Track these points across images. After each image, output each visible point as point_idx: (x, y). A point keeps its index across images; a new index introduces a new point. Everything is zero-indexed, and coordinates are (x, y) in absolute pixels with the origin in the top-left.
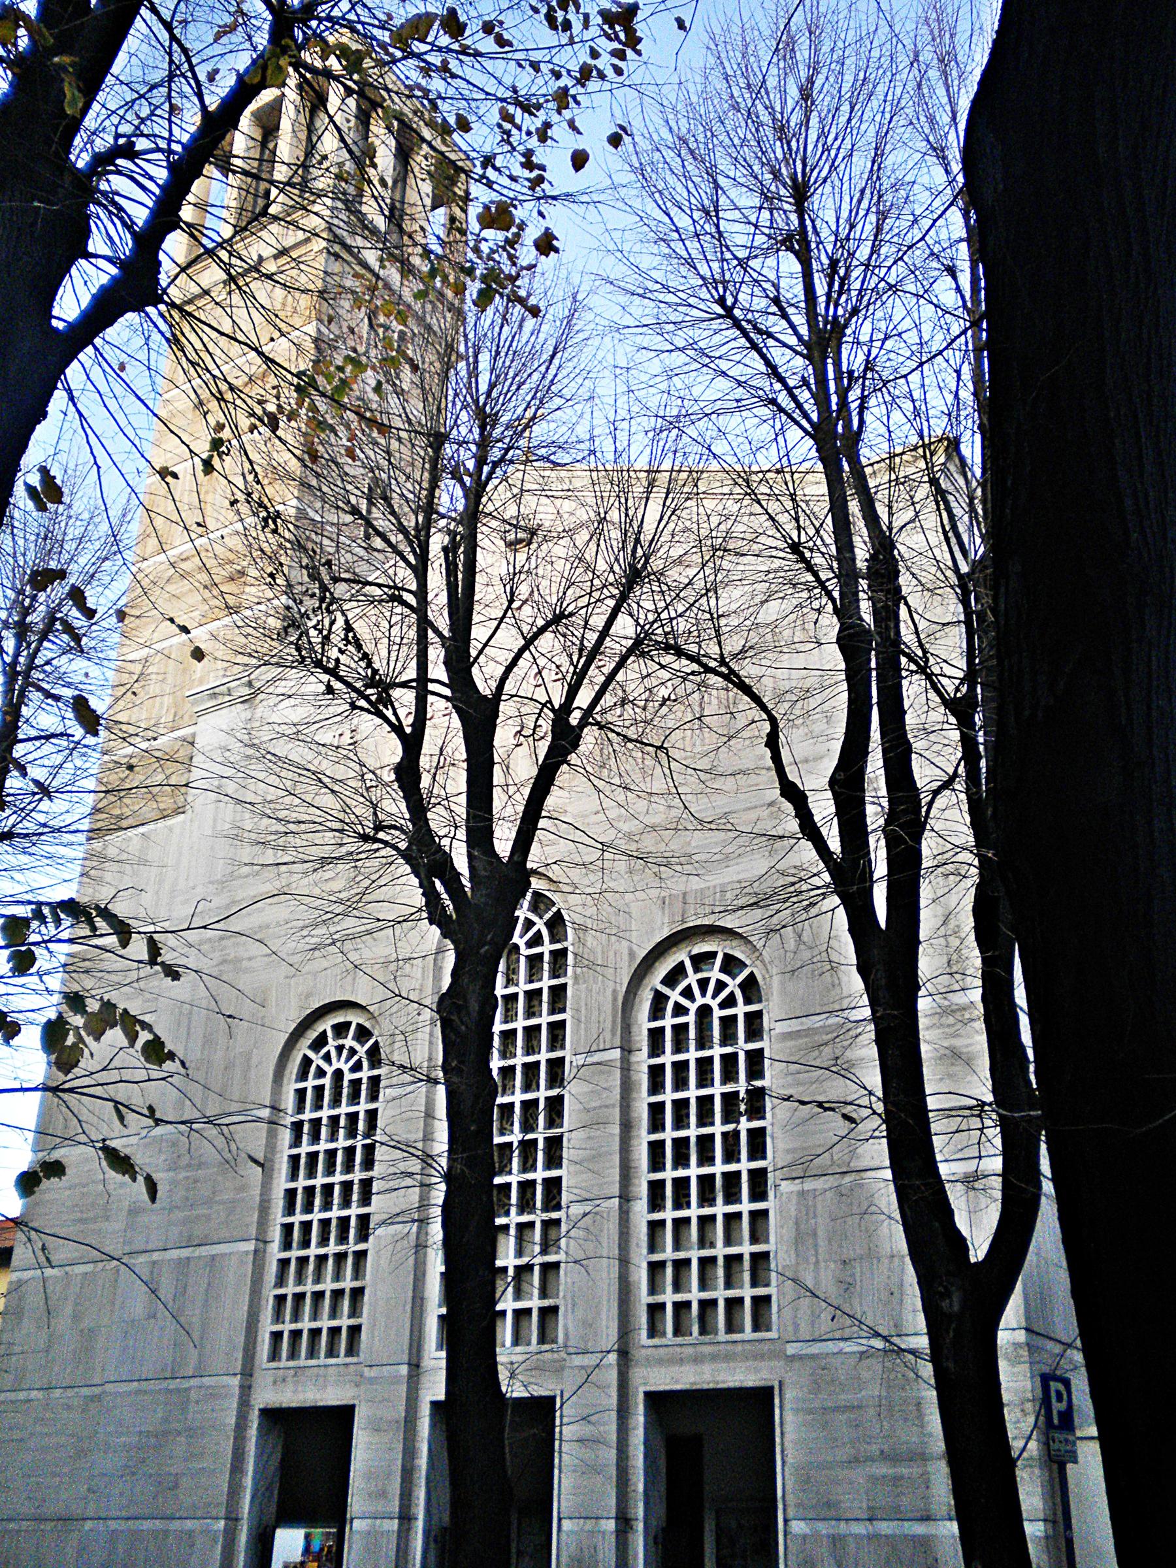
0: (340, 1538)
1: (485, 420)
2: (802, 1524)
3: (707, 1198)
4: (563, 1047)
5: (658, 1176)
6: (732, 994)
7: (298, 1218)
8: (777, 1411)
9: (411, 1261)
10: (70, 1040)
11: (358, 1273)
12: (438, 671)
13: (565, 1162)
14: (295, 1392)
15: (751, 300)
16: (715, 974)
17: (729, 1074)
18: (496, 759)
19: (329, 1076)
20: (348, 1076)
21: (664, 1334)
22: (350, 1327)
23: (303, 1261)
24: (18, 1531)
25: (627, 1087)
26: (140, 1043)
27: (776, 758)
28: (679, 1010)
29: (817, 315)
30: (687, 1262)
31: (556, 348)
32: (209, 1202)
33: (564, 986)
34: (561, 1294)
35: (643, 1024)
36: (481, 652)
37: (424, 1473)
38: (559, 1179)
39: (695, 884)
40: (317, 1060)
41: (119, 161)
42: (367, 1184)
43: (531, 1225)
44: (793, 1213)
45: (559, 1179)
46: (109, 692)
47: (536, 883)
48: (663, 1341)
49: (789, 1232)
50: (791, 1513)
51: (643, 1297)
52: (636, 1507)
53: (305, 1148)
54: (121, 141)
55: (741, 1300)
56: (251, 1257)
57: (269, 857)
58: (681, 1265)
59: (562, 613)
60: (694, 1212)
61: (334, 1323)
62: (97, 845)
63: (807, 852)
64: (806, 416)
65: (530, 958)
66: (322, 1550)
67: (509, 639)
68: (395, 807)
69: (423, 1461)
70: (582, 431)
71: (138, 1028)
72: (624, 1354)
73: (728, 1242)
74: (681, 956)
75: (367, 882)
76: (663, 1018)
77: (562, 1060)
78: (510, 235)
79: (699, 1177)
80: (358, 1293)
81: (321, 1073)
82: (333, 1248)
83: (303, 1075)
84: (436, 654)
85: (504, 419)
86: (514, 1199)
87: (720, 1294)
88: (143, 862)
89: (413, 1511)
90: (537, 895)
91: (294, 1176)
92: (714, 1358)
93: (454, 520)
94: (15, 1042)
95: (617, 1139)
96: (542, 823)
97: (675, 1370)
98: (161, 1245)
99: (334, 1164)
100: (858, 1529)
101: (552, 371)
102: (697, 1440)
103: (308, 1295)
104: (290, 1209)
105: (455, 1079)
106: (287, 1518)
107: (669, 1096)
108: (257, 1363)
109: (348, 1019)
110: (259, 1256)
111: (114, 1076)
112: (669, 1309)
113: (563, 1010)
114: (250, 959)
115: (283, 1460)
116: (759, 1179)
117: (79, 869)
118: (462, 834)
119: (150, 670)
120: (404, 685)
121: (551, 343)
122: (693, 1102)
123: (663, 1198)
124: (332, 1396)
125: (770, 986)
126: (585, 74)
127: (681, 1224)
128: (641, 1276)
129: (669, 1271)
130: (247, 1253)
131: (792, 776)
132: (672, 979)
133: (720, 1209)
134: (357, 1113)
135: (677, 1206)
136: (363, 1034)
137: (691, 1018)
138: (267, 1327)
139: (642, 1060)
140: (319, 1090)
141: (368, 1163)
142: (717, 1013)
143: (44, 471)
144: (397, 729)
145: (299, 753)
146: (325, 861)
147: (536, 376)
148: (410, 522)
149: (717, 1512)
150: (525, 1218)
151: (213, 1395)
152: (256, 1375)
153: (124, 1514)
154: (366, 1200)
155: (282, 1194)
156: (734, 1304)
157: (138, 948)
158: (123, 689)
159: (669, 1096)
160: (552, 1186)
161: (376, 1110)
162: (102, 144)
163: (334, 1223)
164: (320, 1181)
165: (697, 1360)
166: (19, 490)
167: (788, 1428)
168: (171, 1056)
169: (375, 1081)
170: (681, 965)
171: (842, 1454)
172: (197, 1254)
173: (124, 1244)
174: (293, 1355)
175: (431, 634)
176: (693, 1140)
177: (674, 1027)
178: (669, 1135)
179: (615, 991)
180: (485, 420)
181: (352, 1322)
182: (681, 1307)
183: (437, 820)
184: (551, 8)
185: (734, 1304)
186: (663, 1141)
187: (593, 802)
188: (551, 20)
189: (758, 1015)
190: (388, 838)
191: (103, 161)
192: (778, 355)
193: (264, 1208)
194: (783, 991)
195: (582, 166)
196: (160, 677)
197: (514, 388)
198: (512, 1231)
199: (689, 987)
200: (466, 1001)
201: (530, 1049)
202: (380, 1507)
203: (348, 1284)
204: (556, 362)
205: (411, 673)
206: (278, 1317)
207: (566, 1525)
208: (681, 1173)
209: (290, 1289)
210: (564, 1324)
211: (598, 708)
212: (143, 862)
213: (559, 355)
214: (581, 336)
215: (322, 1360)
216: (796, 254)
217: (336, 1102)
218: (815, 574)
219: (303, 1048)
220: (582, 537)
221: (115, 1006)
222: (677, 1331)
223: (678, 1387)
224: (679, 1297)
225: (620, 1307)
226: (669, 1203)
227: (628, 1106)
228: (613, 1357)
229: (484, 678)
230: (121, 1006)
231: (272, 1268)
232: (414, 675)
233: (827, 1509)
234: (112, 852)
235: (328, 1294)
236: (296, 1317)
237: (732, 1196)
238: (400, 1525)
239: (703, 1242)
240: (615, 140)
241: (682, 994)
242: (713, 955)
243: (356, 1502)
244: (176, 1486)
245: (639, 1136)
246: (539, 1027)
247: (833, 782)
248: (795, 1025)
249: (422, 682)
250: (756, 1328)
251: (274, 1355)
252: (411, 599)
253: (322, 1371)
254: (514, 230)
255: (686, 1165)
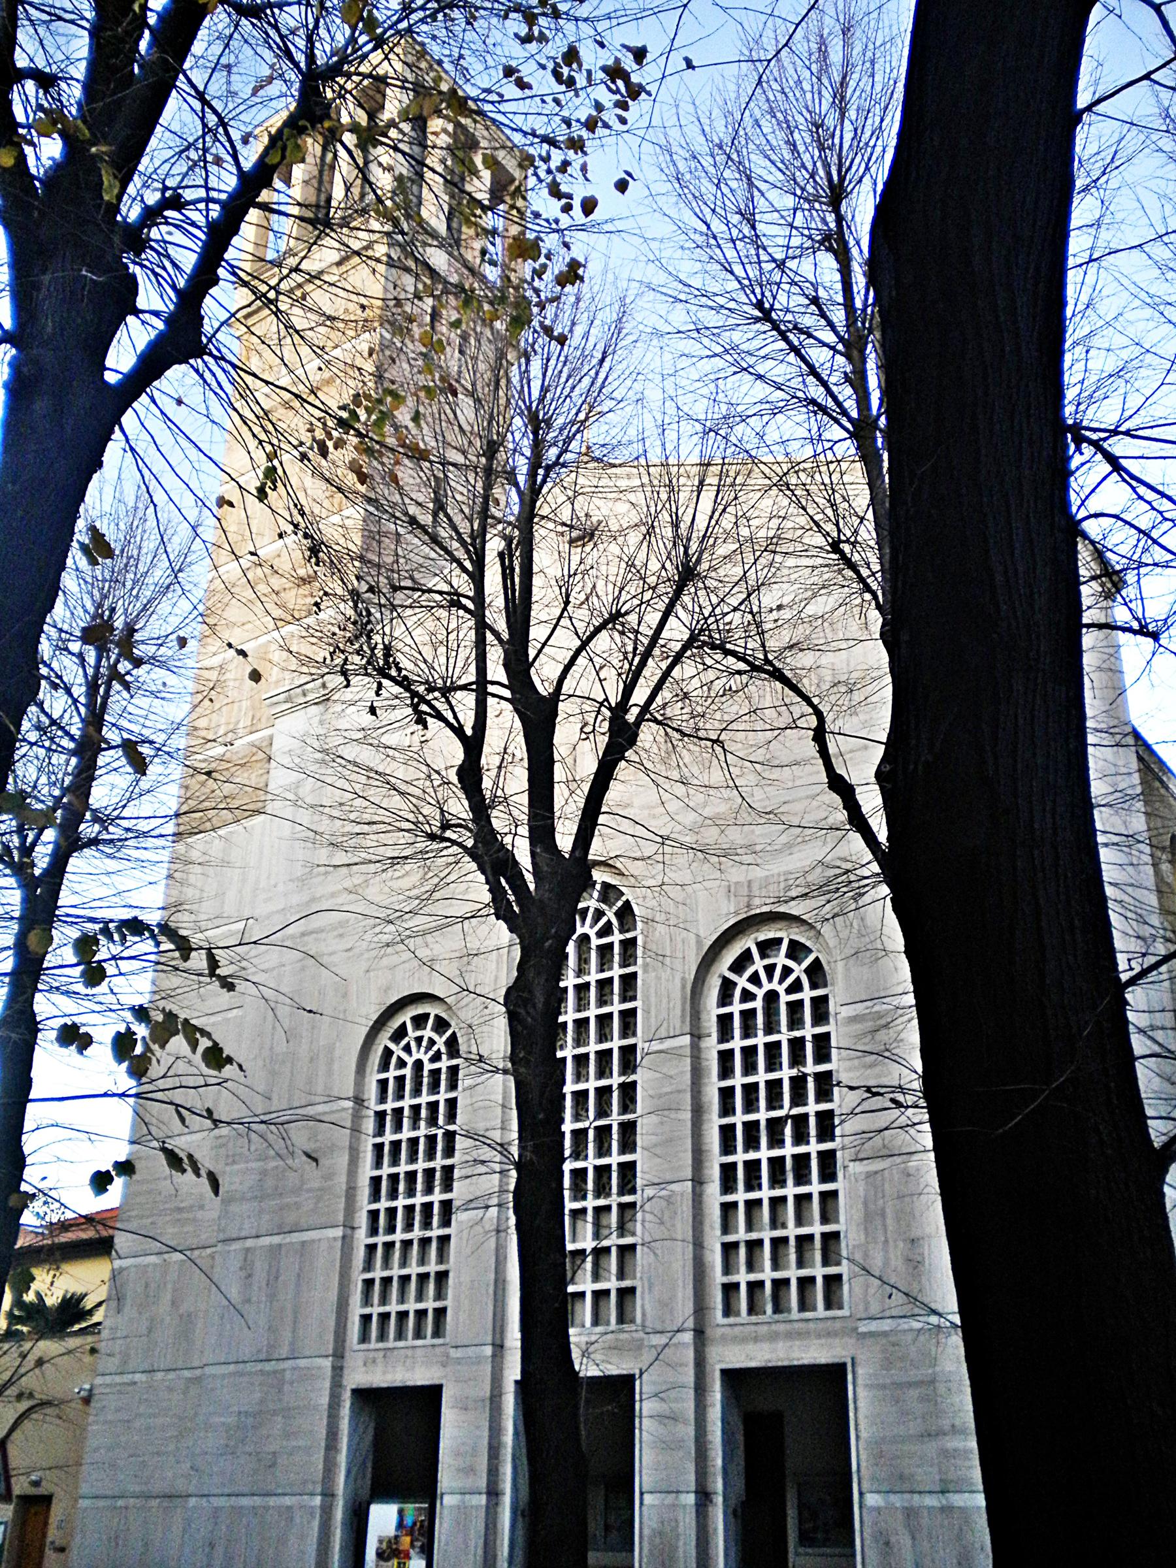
0: (431, 1514)
1: (537, 423)
2: (876, 1496)
3: (777, 1179)
4: (634, 1034)
5: (730, 1159)
6: (798, 980)
7: (383, 1204)
8: (850, 1388)
9: (492, 1243)
10: (139, 1050)
11: (442, 1257)
12: (496, 671)
13: (639, 1149)
14: (384, 1373)
15: (789, 301)
16: (781, 959)
17: (797, 1058)
18: (556, 757)
19: (409, 1066)
20: (428, 1067)
21: (738, 1314)
22: (435, 1310)
23: (389, 1246)
24: (126, 1508)
25: (697, 1073)
26: (200, 1049)
27: (824, 753)
28: (747, 996)
29: (855, 310)
30: (760, 1242)
31: (604, 352)
32: (297, 1191)
33: (634, 975)
34: (638, 1275)
35: (712, 1010)
36: (540, 651)
37: (509, 1450)
38: (634, 1163)
39: (758, 873)
40: (397, 1050)
41: (167, 213)
42: (448, 1171)
43: (608, 1208)
44: (862, 1193)
45: (634, 1163)
46: (189, 699)
47: (598, 876)
48: (761, 1318)
49: (858, 1215)
50: (866, 1486)
51: (718, 1278)
52: (715, 1482)
53: (389, 1137)
54: (168, 194)
55: (812, 1279)
56: (339, 1243)
57: (340, 858)
58: (754, 1246)
59: (618, 611)
60: (765, 1193)
61: (421, 1306)
62: (180, 847)
63: (856, 841)
64: (845, 413)
65: (600, 948)
66: (414, 1524)
67: (566, 641)
68: (459, 807)
69: (508, 1438)
70: (632, 433)
71: (198, 1035)
72: (700, 1333)
73: (799, 1222)
74: (748, 942)
75: (436, 880)
76: (731, 1004)
77: (633, 1047)
78: (537, 266)
79: (770, 1160)
80: (442, 1276)
81: (402, 1064)
82: (417, 1233)
83: (384, 1067)
84: (495, 655)
85: (560, 421)
86: (590, 1185)
87: (792, 1273)
88: (225, 863)
89: (501, 1486)
90: (606, 886)
91: (378, 1164)
92: (789, 1336)
93: (510, 523)
94: (89, 1051)
95: (689, 1124)
96: (602, 819)
97: (750, 1347)
98: (254, 1233)
99: (416, 1152)
100: (931, 1501)
101: (602, 376)
102: (777, 1418)
103: (395, 1280)
104: (375, 1196)
105: (522, 1070)
106: (382, 1491)
107: (738, 1080)
108: (348, 1344)
109: (778, 935)
110: (347, 1242)
111: (176, 1082)
112: (743, 1288)
113: (634, 998)
114: (331, 954)
115: (376, 1436)
116: (828, 1160)
117: (165, 872)
118: (524, 830)
119: (228, 675)
120: (464, 687)
121: (600, 347)
122: (762, 1086)
123: (735, 1180)
124: (420, 1377)
125: (834, 971)
126: (591, 125)
127: (753, 1206)
128: (715, 1258)
129: (742, 1251)
130: (335, 1239)
131: (841, 771)
132: (738, 966)
133: (790, 1190)
134: (437, 1102)
135: (749, 1188)
136: (441, 1025)
137: (758, 1004)
138: (356, 1310)
139: (712, 1046)
140: (400, 1080)
141: (449, 1151)
142: (784, 998)
143: (93, 530)
144: (458, 731)
145: (367, 756)
146: (395, 860)
147: (587, 381)
148: (464, 527)
149: (799, 1485)
150: (602, 1202)
151: (307, 1376)
152: (347, 1354)
153: (227, 1491)
154: (448, 1186)
155: (367, 1182)
156: (806, 1283)
157: (198, 961)
158: (200, 697)
159: (738, 1080)
160: (628, 1170)
161: (455, 1099)
162: (152, 198)
163: (418, 1208)
164: (403, 1168)
165: (773, 1337)
166: (75, 544)
167: (861, 1404)
168: (229, 1060)
169: (454, 1071)
170: (748, 952)
171: (914, 1427)
172: (288, 1240)
173: (219, 1230)
174: (382, 1337)
175: (489, 637)
176: (763, 1124)
177: (742, 1012)
178: (739, 1118)
179: (683, 979)
180: (537, 423)
181: (438, 1304)
182: (755, 1287)
183: (499, 821)
184: (557, 65)
185: (806, 1283)
186: (734, 1125)
187: (652, 795)
188: (557, 75)
189: (824, 999)
190: (454, 836)
191: (152, 215)
192: (819, 356)
193: (351, 1193)
194: (847, 977)
195: (592, 212)
196: (237, 684)
197: (568, 390)
198: (590, 1217)
199: (756, 973)
200: (530, 992)
201: (603, 1037)
202: (468, 1483)
203: (432, 1267)
204: (606, 364)
205: (471, 676)
206: (367, 1300)
207: (648, 1498)
208: (752, 1155)
209: (378, 1274)
210: (642, 1304)
211: (654, 705)
212: (225, 863)
213: (608, 359)
214: (631, 338)
215: (429, 1341)
216: (835, 253)
217: (417, 1092)
218: (857, 573)
219: (384, 1040)
220: (634, 538)
221: (176, 1016)
222: (751, 1310)
223: (753, 1364)
224: (753, 1277)
225: (695, 1288)
226: (741, 1185)
227: (699, 1092)
228: (688, 1337)
229: (544, 675)
230: (182, 1016)
231: (360, 1254)
232: (473, 679)
233: (899, 1483)
234: (195, 855)
235: (414, 1278)
236: (384, 1300)
237: (802, 1177)
238: (488, 1501)
239: (775, 1223)
240: (622, 186)
241: (750, 980)
242: (779, 941)
243: (445, 1479)
244: (273, 1465)
245: (710, 1120)
246: (610, 1015)
247: (879, 775)
248: (860, 1008)
249: (481, 686)
250: (829, 1306)
251: (364, 1338)
252: (470, 605)
253: (409, 1352)
254: (542, 260)
255: (757, 1148)
